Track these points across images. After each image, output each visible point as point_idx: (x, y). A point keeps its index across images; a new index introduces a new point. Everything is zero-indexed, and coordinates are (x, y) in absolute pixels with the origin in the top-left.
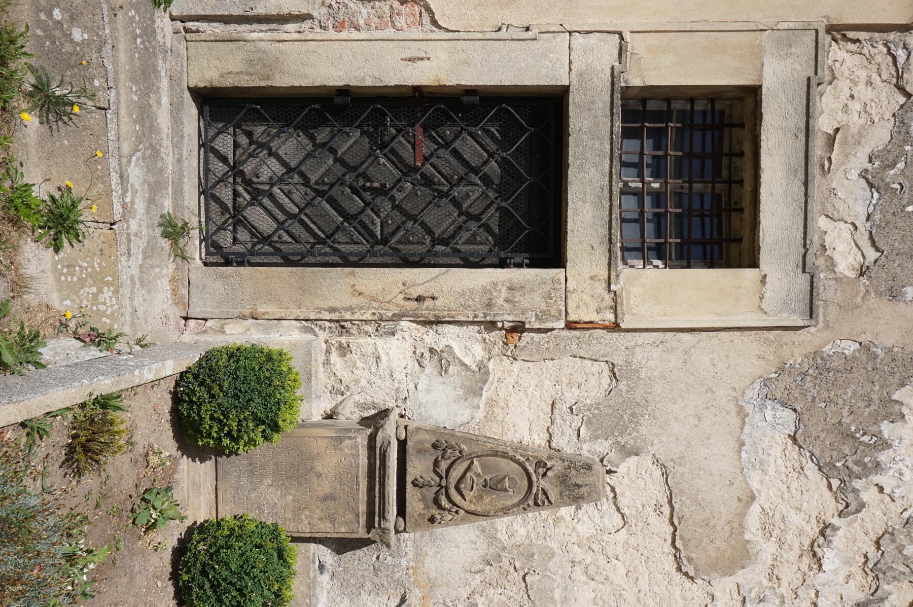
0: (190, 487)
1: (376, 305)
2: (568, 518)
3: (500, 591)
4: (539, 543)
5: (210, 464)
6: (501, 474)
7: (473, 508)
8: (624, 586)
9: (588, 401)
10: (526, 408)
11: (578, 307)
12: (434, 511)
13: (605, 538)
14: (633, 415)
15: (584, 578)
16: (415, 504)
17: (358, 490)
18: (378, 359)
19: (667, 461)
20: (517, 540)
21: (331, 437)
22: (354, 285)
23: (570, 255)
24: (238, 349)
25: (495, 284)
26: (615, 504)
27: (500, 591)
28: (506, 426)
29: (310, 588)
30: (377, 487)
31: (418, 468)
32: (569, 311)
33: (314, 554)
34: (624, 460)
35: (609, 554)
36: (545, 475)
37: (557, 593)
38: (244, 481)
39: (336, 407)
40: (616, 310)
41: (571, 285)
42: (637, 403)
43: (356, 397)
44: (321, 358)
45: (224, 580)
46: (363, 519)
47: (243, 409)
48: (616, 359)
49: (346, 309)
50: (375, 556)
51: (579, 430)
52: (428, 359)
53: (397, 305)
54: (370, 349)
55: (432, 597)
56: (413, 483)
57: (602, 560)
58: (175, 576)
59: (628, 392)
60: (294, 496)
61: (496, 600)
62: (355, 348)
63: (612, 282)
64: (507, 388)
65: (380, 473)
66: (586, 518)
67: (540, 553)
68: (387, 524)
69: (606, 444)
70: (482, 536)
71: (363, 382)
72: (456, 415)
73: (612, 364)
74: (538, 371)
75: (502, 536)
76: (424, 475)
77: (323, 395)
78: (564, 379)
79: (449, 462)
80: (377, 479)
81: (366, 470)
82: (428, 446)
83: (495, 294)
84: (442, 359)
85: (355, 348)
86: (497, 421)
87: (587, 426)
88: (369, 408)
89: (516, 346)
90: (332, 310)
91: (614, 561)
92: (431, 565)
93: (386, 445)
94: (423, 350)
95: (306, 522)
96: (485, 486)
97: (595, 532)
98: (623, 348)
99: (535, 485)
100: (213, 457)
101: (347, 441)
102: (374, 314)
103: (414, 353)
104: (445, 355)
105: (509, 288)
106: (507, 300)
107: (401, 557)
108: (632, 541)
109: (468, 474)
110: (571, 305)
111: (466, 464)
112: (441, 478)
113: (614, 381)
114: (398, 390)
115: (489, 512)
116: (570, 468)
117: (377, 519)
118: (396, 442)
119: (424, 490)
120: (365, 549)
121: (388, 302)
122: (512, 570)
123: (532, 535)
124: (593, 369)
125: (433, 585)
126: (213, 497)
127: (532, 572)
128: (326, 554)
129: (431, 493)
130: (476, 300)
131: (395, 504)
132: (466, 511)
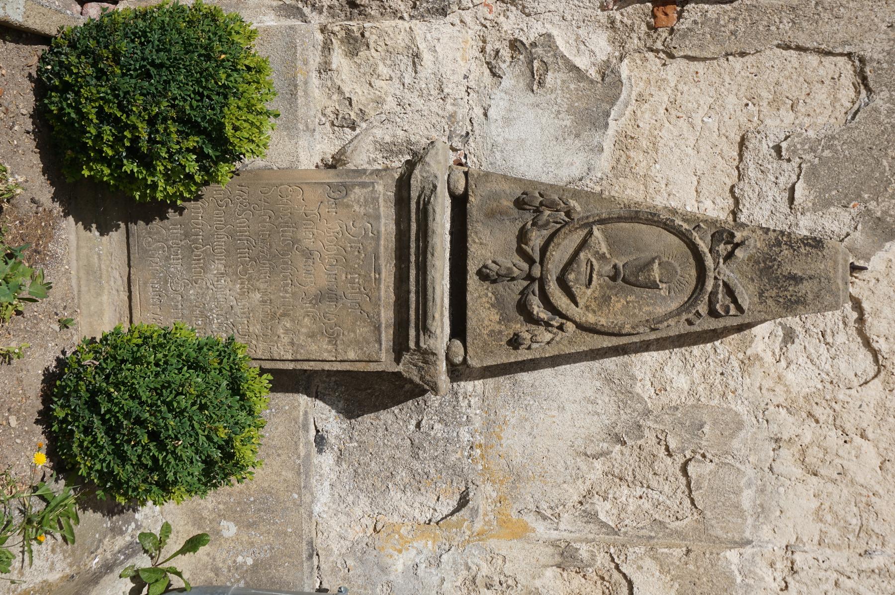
0: (82, 274)
2: (768, 358)
3: (639, 491)
4: (712, 403)
5: (117, 237)
6: (646, 256)
7: (591, 318)
8: (877, 488)
9: (811, 134)
10: (690, 151)
12: (520, 327)
13: (841, 396)
15: (798, 472)
16: (484, 314)
17: (378, 281)
18: (416, 57)
20: (673, 397)
21: (329, 184)
26: (861, 332)
27: (639, 491)
28: (653, 185)
29: (299, 474)
30: (413, 273)
31: (489, 246)
33: (306, 413)
34: (881, 247)
35: (848, 427)
36: (730, 256)
37: (747, 499)
38: (177, 267)
39: (342, 151)
43: (378, 133)
44: (315, 59)
45: (127, 415)
46: (387, 336)
47: (155, 97)
48: (866, 46)
50: (414, 422)
51: (792, 190)
52: (508, 60)
54: (401, 40)
55: (515, 499)
56: (479, 273)
57: (833, 438)
58: (45, 417)
60: (265, 293)
61: (631, 508)
62: (374, 37)
64: (654, 113)
65: (417, 247)
66: (802, 360)
67: (715, 423)
68: (431, 342)
69: (845, 217)
70: (607, 390)
71: (390, 104)
72: (559, 165)
73: (862, 60)
74: (715, 78)
75: (644, 389)
76: (500, 259)
77: (319, 129)
78: (765, 94)
79: (546, 233)
80: (413, 258)
81: (392, 245)
82: (508, 203)
85: (374, 37)
86: (635, 176)
87: (807, 181)
88: (401, 152)
89: (672, 31)
91: (858, 440)
92: (513, 441)
93: (428, 192)
94: (497, 45)
95: (286, 340)
96: (614, 278)
97: (820, 386)
98: (883, 27)
99: (711, 274)
100: (122, 225)
101: (357, 190)
103: (483, 50)
104: (539, 50)
107: (460, 424)
109: (582, 255)
111: (577, 237)
112: (531, 261)
113: (864, 92)
114: (452, 116)
115: (622, 326)
116: (778, 243)
117: (412, 333)
118: (448, 202)
119: (500, 287)
120: (396, 409)
122: (662, 453)
123: (700, 389)
124: (822, 72)
125: (517, 477)
126: (124, 296)
127: (699, 457)
128: (323, 415)
129: (512, 291)
131: (447, 314)
132: (580, 326)
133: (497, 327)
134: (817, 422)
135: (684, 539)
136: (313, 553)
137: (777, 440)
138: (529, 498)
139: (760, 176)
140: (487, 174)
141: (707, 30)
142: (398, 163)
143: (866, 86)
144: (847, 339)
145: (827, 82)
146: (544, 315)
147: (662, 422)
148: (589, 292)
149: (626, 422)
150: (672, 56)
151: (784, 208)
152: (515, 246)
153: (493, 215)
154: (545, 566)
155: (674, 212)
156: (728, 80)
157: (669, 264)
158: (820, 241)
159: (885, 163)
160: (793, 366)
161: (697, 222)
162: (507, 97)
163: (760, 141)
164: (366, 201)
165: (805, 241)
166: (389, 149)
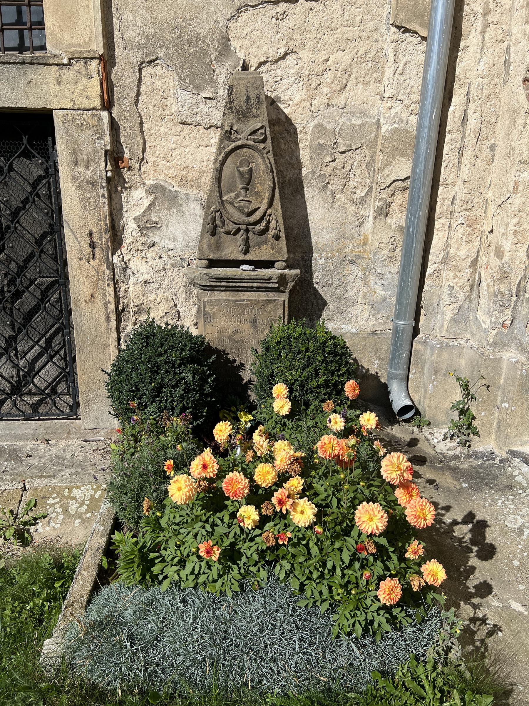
1: (101, 283)
4: (309, 139)
6: (237, 174)
7: (266, 201)
8: (353, 53)
11: (88, 97)
14: (189, 42)
15: (344, 95)
19: (233, 6)
22: (86, 301)
23: (39, 105)
24: (112, 396)
25: (74, 178)
30: (244, 285)
31: (232, 250)
32: (92, 106)
37: (356, 121)
40: (86, 58)
41: (69, 105)
42: (178, 37)
48: (135, 61)
49: (107, 308)
53: (99, 265)
54: (139, 288)
59: (167, 48)
63: (60, 62)
67: (319, 138)
69: (218, 71)
73: (142, 63)
74: (152, 139)
76: (238, 245)
78: (159, 113)
83: (82, 178)
84: (147, 226)
87: (201, 91)
90: (108, 319)
99: (245, 142)
101: (207, 309)
102: (108, 285)
103: (142, 250)
104: (141, 224)
105: (76, 165)
106: (87, 167)
108: (311, 44)
110: (86, 104)
112: (239, 230)
116: (231, 108)
117: (270, 285)
119: (251, 244)
121: (98, 273)
130: (89, 195)
133: (270, 246)
134: (320, 84)
135: (375, 153)
136: (374, 333)
137: (328, 105)
138: (353, 231)
139: (199, 115)
140: (199, 250)
141: (130, 141)
142: (196, 291)
143: (155, 60)
144: (279, 69)
145: (153, 80)
146: (264, 224)
147: (318, 164)
148: (253, 202)
149: (317, 183)
150: (143, 159)
151: (214, 102)
152: (233, 237)
153: (218, 247)
154: (385, 223)
155: (216, 160)
156: (153, 131)
157: (240, 162)
158: (229, 87)
159: (192, 50)
160: (292, 97)
161: (220, 150)
162: (164, 240)
163: (183, 115)
164: (212, 305)
165: (230, 94)
166: (189, 295)
